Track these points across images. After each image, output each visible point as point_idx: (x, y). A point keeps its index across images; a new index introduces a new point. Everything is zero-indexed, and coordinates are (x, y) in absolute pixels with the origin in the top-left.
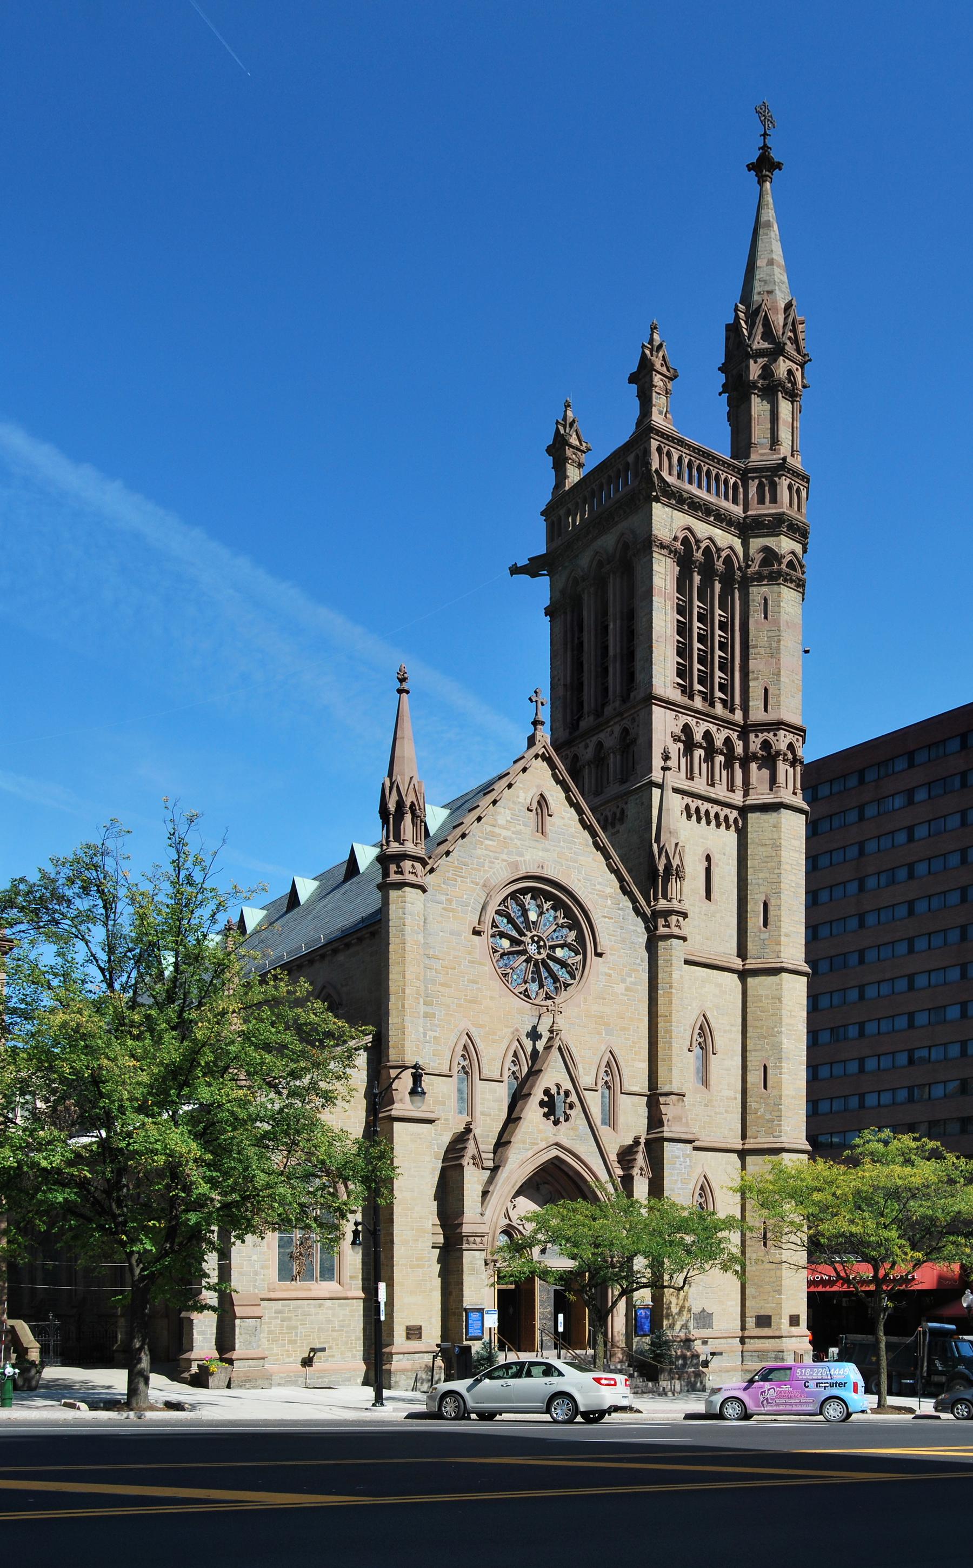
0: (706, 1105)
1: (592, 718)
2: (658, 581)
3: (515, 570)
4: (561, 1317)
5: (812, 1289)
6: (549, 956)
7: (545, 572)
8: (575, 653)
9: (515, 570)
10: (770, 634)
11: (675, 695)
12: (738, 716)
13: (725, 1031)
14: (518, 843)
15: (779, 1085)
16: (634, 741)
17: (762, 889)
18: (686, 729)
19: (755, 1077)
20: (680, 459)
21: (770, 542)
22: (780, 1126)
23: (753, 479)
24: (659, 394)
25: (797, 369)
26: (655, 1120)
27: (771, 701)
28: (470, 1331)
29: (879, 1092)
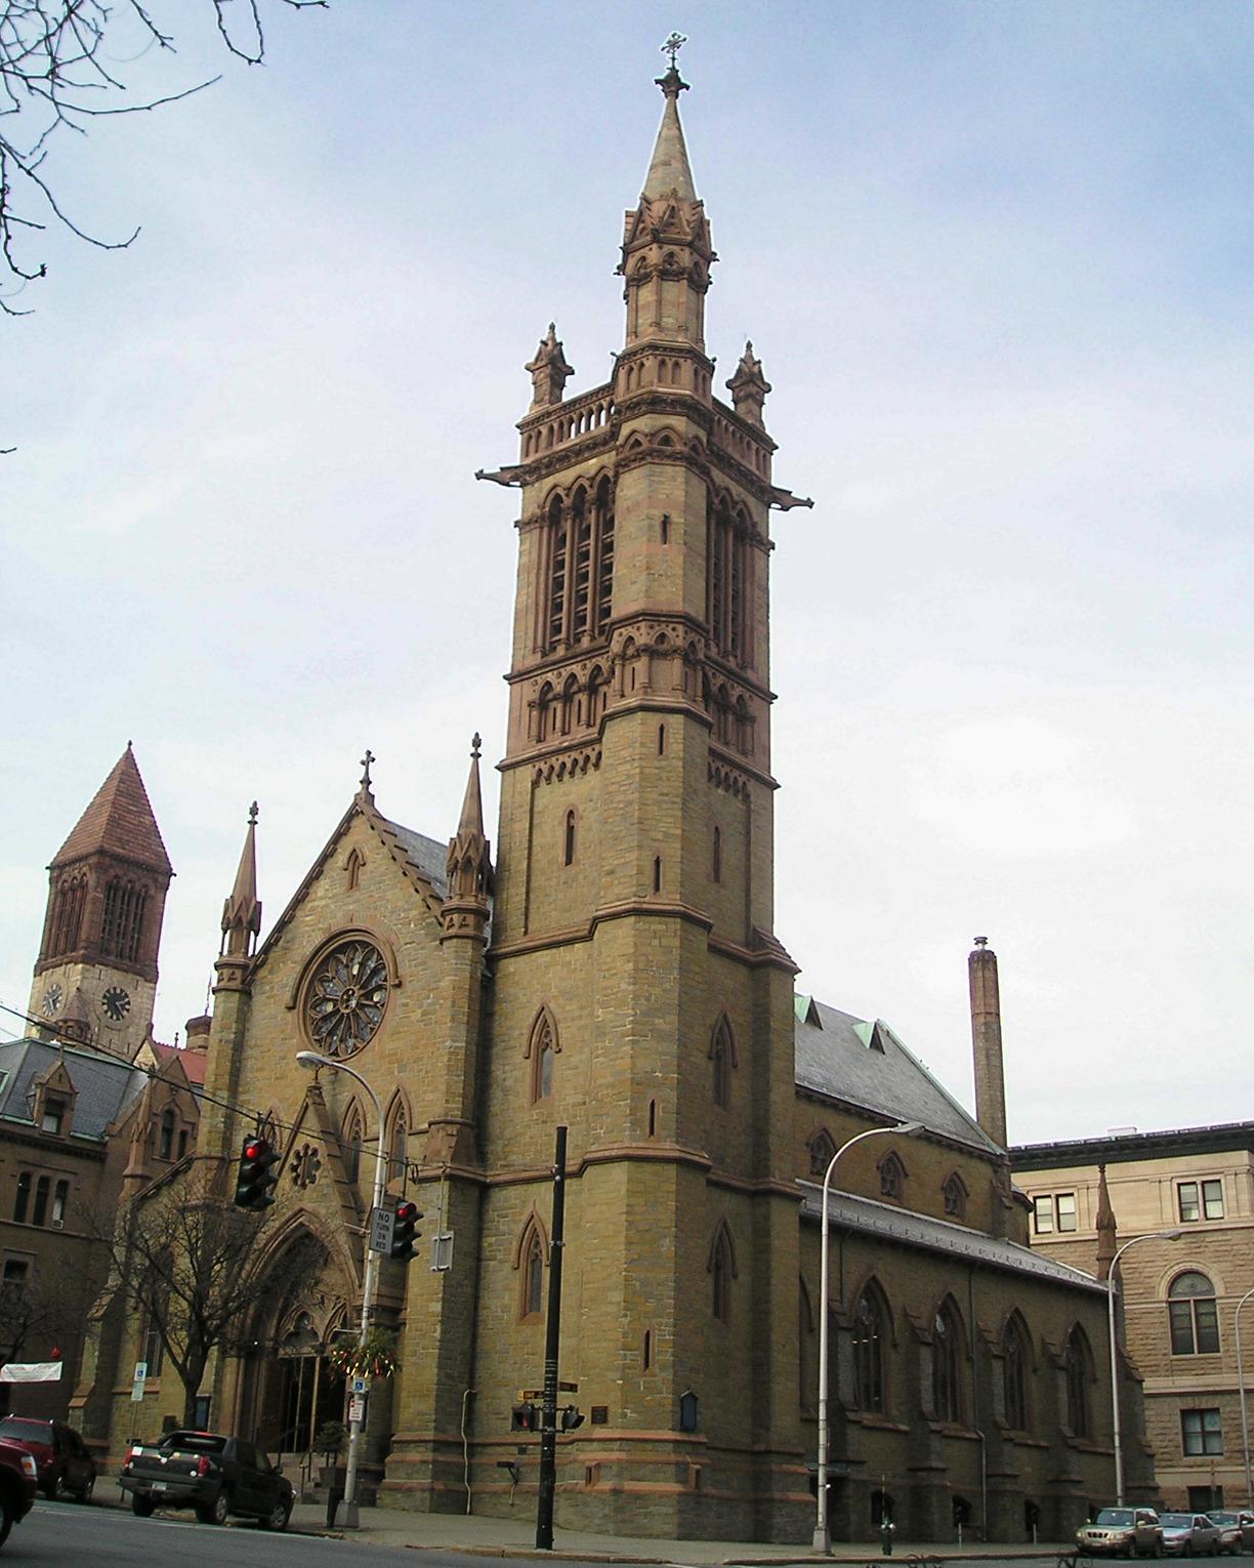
0: (544, 1122)
14: (332, 906)
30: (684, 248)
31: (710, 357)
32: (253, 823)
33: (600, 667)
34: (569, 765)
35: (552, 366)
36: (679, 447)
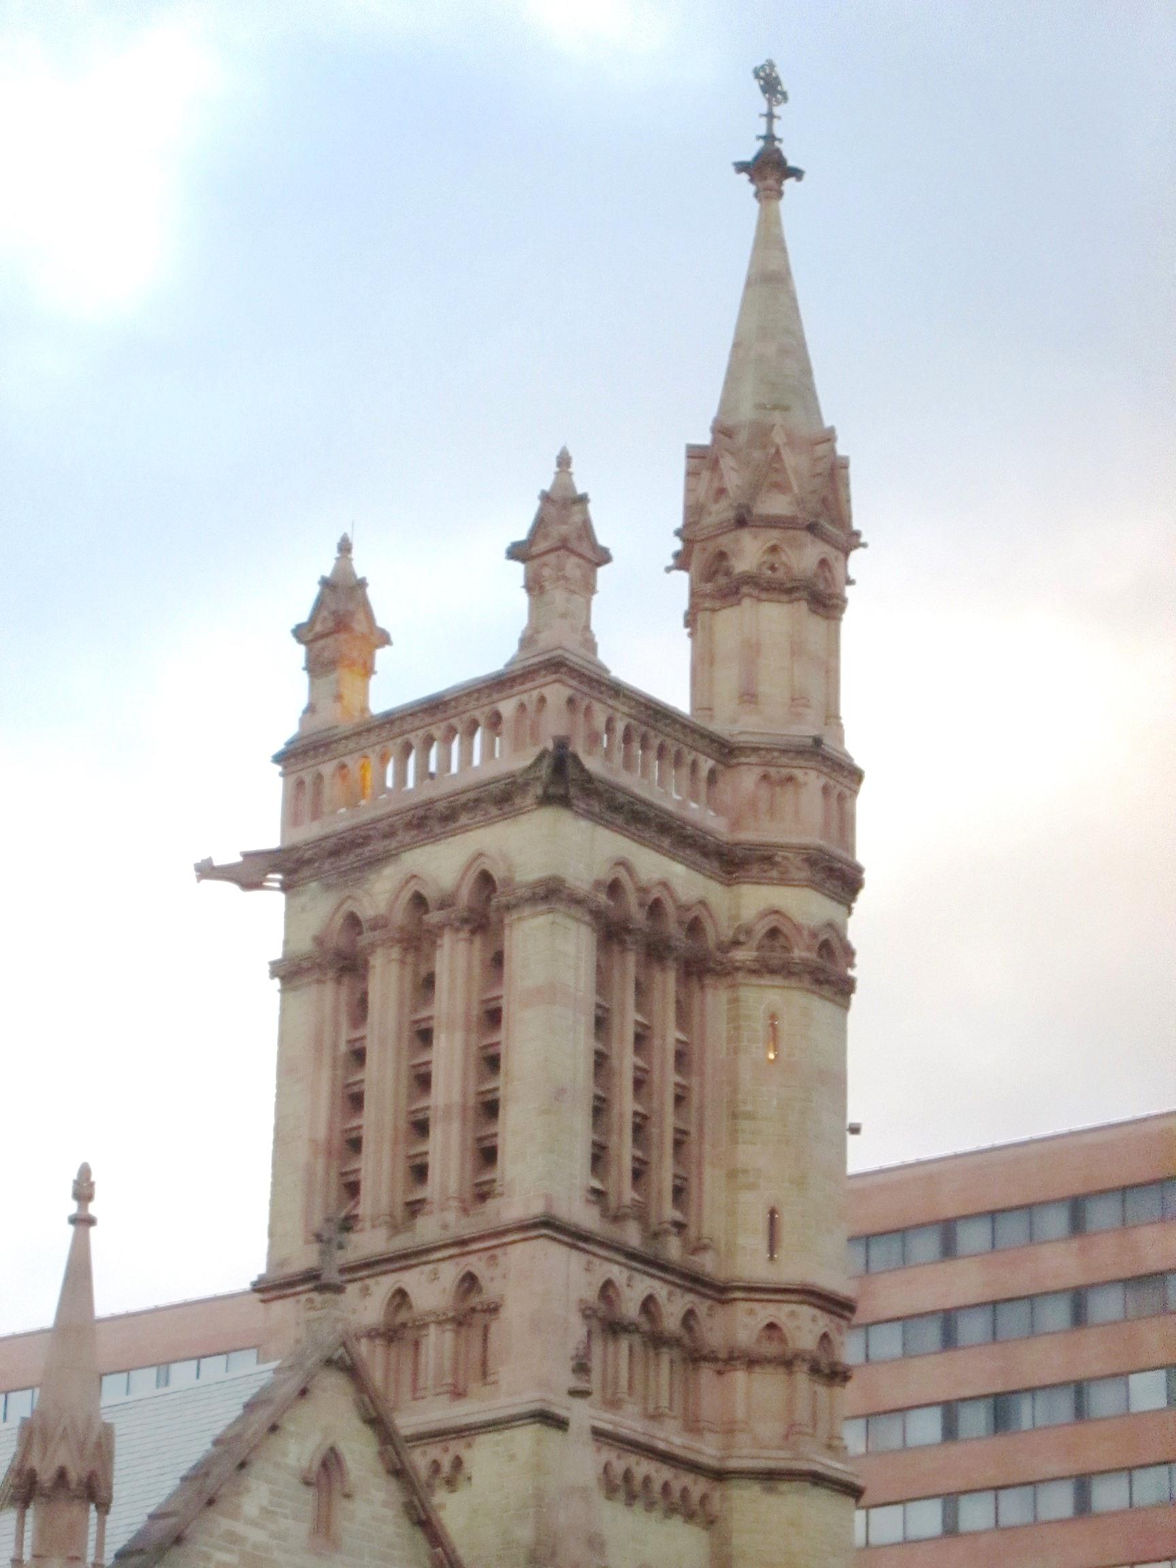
3: (207, 871)
9: (207, 871)
16: (493, 1309)
20: (610, 723)
25: (837, 558)
31: (852, 1119)
32: (83, 1222)
34: (446, 1467)
35: (339, 628)
36: (798, 953)
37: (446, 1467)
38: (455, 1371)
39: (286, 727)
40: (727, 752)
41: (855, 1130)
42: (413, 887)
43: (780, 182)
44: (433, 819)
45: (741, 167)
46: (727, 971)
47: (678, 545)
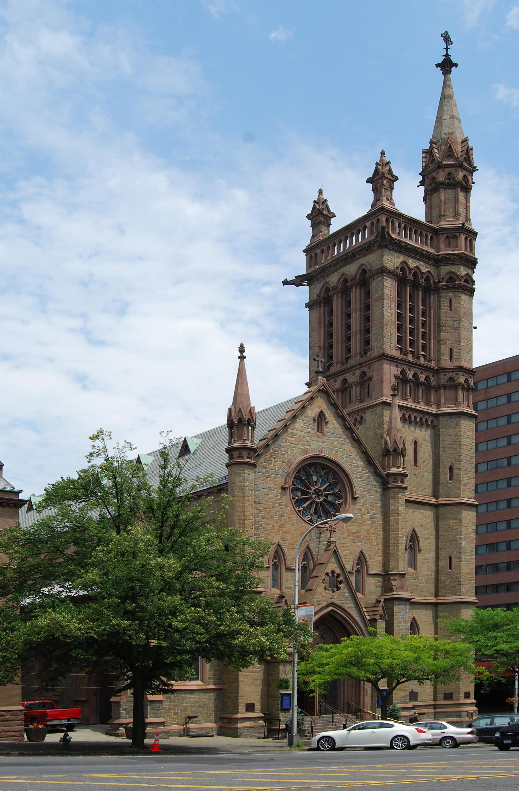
0: (414, 579)
1: (339, 365)
2: (387, 291)
3: (285, 283)
4: (511, 748)
5: (475, 237)
6: (324, 500)
7: (306, 284)
8: (326, 328)
9: (285, 283)
10: (454, 319)
11: (396, 354)
12: (433, 364)
13: (426, 538)
14: (308, 438)
15: (459, 567)
16: (370, 379)
17: (449, 459)
18: (403, 372)
19: (444, 563)
21: (453, 268)
22: (460, 590)
23: (443, 234)
24: (387, 189)
26: (387, 588)
27: (454, 356)
28: (284, 705)
29: (487, 421)
30: (457, 168)
32: (242, 358)
33: (365, 373)
34: (359, 419)
35: (320, 215)
37: (359, 419)
38: (361, 397)
39: (306, 242)
40: (436, 232)
41: (475, 328)
42: (344, 277)
43: (450, 68)
44: (348, 258)
45: (438, 65)
46: (438, 290)
47: (420, 178)
